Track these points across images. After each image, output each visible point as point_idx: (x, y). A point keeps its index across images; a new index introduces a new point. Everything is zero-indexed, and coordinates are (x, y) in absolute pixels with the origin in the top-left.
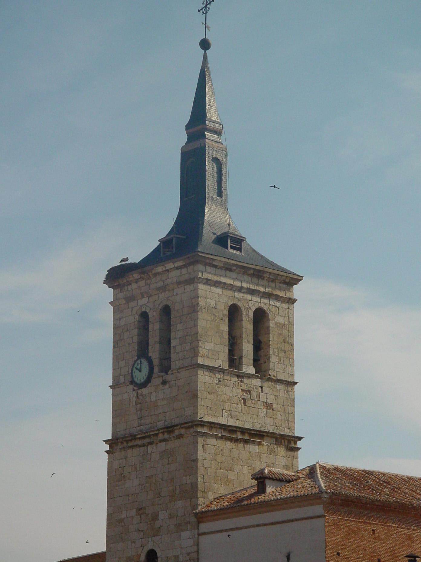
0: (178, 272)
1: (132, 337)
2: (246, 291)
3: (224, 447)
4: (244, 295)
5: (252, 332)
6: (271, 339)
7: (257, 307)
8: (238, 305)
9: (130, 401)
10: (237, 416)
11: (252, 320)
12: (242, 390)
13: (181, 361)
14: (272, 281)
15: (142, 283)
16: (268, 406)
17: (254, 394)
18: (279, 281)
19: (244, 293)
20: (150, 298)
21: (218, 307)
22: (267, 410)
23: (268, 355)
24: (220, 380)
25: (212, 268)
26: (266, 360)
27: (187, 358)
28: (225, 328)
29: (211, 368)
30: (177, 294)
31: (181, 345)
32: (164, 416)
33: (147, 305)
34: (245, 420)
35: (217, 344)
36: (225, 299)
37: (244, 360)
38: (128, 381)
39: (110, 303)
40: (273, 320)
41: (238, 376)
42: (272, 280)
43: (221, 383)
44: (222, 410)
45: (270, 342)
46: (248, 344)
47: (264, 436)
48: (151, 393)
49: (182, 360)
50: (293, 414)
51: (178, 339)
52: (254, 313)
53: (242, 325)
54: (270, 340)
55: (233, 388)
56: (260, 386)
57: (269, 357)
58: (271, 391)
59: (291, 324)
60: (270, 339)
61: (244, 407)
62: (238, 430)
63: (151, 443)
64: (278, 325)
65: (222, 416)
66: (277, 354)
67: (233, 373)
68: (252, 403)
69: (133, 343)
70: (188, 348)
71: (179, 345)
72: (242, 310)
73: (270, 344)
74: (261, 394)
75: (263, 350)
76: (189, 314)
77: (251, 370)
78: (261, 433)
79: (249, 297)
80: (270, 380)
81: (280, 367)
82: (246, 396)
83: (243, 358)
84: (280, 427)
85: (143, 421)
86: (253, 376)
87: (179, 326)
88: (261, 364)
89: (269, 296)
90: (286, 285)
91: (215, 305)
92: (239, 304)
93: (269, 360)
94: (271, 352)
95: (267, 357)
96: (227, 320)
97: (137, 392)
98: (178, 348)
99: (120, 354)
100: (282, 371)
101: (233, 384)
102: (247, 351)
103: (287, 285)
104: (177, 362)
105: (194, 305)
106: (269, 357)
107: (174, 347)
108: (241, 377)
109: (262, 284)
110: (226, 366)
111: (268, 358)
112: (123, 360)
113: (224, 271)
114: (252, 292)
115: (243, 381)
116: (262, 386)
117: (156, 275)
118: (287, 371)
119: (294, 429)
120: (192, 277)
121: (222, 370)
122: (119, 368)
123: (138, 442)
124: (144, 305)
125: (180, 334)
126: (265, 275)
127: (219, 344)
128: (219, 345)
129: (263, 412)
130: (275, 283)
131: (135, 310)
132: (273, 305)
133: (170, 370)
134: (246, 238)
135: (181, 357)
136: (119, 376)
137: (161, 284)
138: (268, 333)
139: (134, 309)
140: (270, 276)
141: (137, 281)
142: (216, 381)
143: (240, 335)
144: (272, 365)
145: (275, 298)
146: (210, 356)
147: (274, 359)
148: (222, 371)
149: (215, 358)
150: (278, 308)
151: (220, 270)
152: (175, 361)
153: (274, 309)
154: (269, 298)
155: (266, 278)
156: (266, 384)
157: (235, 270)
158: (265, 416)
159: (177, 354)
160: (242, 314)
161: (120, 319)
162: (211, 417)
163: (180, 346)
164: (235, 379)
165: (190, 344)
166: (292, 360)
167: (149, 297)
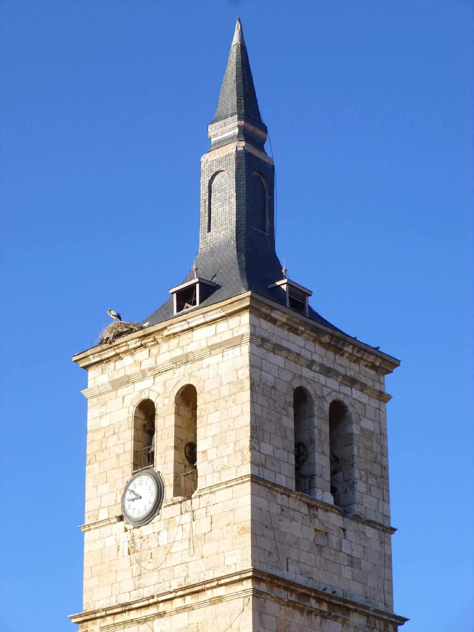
0: (208, 330)
1: (124, 444)
2: (319, 369)
3: (291, 622)
4: (316, 375)
5: (329, 437)
6: (356, 453)
7: (334, 399)
8: (307, 390)
9: (118, 549)
10: (308, 572)
11: (328, 417)
12: (316, 530)
13: (217, 475)
14: (355, 362)
15: (142, 354)
16: (352, 561)
17: (334, 539)
18: (366, 363)
19: (315, 372)
20: (157, 379)
21: (278, 387)
22: (353, 569)
23: (351, 479)
24: (283, 507)
25: (269, 324)
26: (348, 488)
27: (229, 468)
28: (289, 423)
29: (270, 486)
30: (208, 366)
31: (217, 447)
32: (184, 568)
33: (151, 388)
34: (322, 580)
35: (277, 448)
36: (289, 377)
37: (318, 480)
38: (116, 516)
39: (356, 337)
40: (358, 423)
41: (310, 506)
42: (355, 358)
43: (285, 512)
44: (287, 559)
45: (355, 457)
46: (322, 456)
47: (349, 609)
48: (159, 533)
49: (219, 472)
50: (390, 580)
51: (210, 439)
52: (330, 407)
53: (313, 423)
54: (354, 455)
55: (302, 524)
56: (342, 527)
57: (354, 482)
58: (358, 538)
59: (382, 434)
60: (355, 454)
61: (320, 560)
62: (313, 594)
63: (160, 615)
64: (366, 432)
65: (287, 570)
66: (364, 479)
67: (303, 499)
68: (331, 555)
69: (125, 452)
70: (230, 451)
71: (213, 448)
72: (314, 400)
73: (355, 460)
74: (343, 540)
75: (341, 473)
76: (231, 395)
77: (329, 499)
78: (346, 605)
79: (322, 379)
80: (357, 518)
81: (370, 502)
82: (321, 541)
83: (317, 477)
84: (372, 600)
85: (143, 581)
86: (331, 508)
87: (214, 417)
88: (339, 494)
89: (352, 382)
90: (375, 372)
91: (274, 383)
92: (308, 388)
93: (354, 487)
94: (357, 475)
95: (349, 483)
96: (291, 410)
97: (133, 533)
98: (211, 455)
99: (100, 473)
100: (373, 508)
101: (303, 518)
102: (323, 466)
103: (376, 371)
104: (209, 477)
105: (242, 380)
106: (354, 483)
107: (203, 452)
108: (314, 509)
109: (340, 363)
110: (292, 485)
111: (352, 485)
112: (107, 482)
113: (287, 332)
114: (328, 372)
115: (317, 515)
116: (344, 528)
117: (170, 337)
118: (380, 509)
119: (392, 606)
120: (236, 335)
121: (286, 491)
122: (98, 497)
123: (133, 615)
124: (147, 388)
125: (214, 430)
126: (346, 349)
127: (280, 449)
128: (280, 450)
129: (347, 572)
130: (359, 365)
131: (128, 401)
132: (357, 400)
133: (196, 490)
134: (312, 292)
135: (217, 468)
136: (99, 509)
137: (179, 352)
138: (351, 444)
139: (126, 399)
140: (353, 351)
141: (131, 352)
142: (275, 509)
143: (310, 439)
144: (358, 496)
145: (360, 388)
146: (269, 465)
147: (361, 487)
148: (286, 492)
149: (275, 469)
150: (364, 406)
151: (280, 329)
152: (205, 476)
153: (358, 406)
154: (352, 388)
155: (346, 355)
156: (351, 526)
157: (302, 332)
158: (351, 579)
159: (209, 463)
160: (312, 406)
161: (101, 417)
162: (271, 569)
163: (215, 448)
164: (305, 509)
165: (235, 444)
166: (387, 492)
167: (155, 376)
